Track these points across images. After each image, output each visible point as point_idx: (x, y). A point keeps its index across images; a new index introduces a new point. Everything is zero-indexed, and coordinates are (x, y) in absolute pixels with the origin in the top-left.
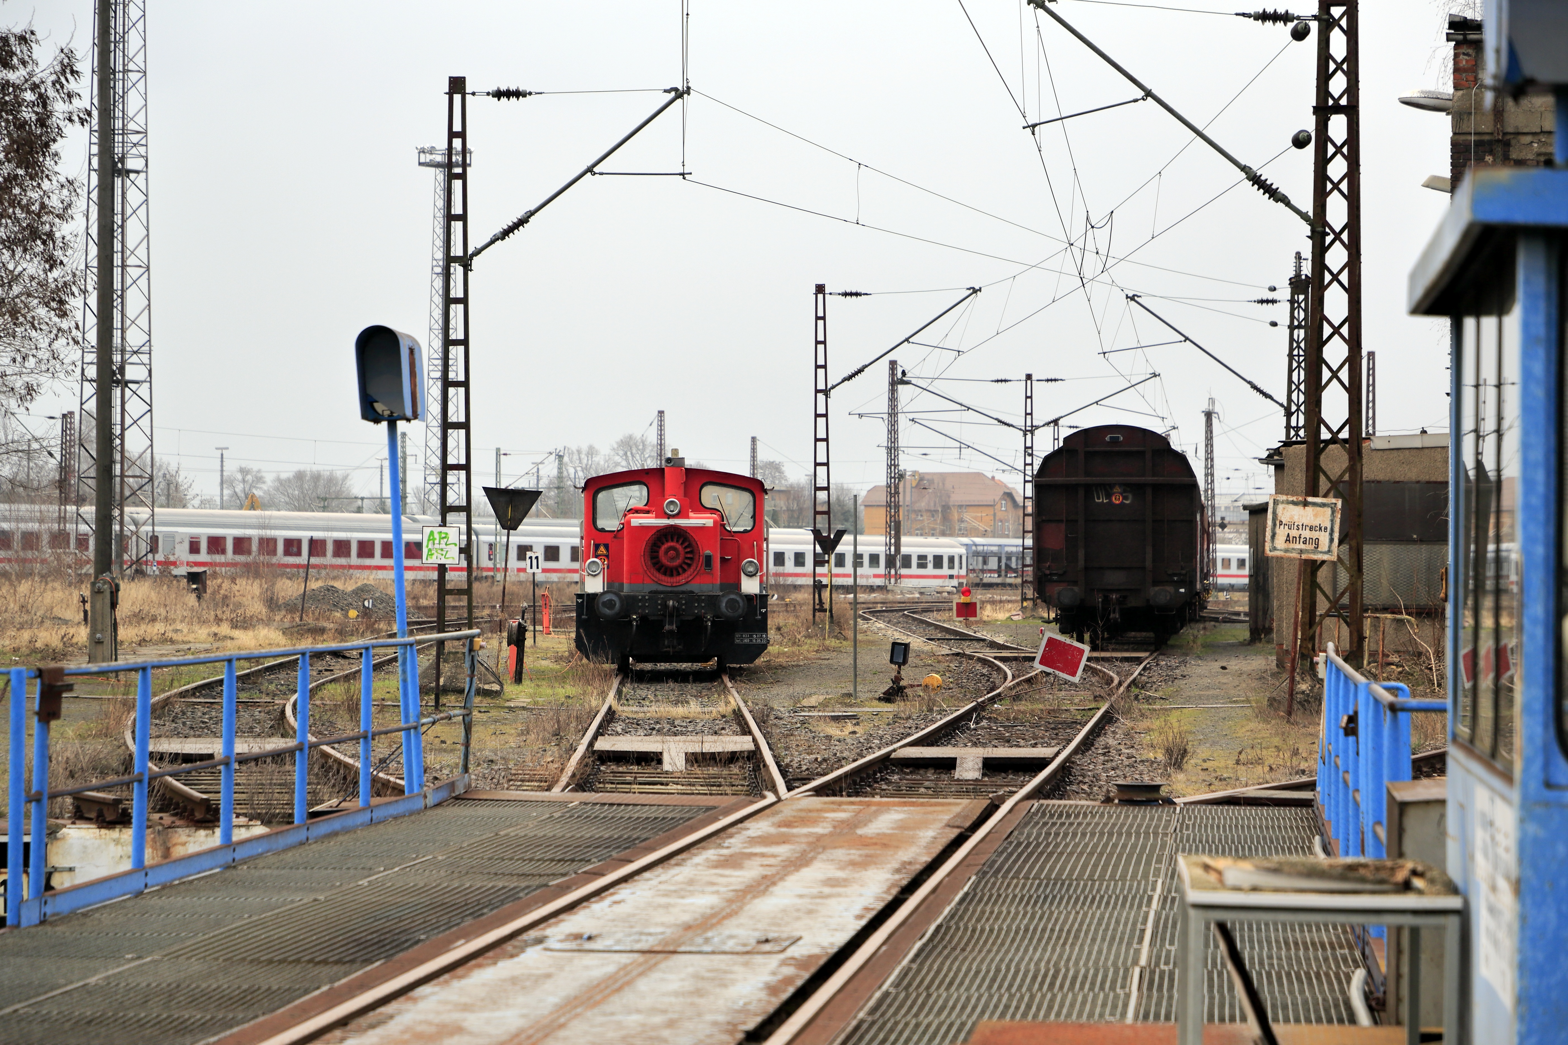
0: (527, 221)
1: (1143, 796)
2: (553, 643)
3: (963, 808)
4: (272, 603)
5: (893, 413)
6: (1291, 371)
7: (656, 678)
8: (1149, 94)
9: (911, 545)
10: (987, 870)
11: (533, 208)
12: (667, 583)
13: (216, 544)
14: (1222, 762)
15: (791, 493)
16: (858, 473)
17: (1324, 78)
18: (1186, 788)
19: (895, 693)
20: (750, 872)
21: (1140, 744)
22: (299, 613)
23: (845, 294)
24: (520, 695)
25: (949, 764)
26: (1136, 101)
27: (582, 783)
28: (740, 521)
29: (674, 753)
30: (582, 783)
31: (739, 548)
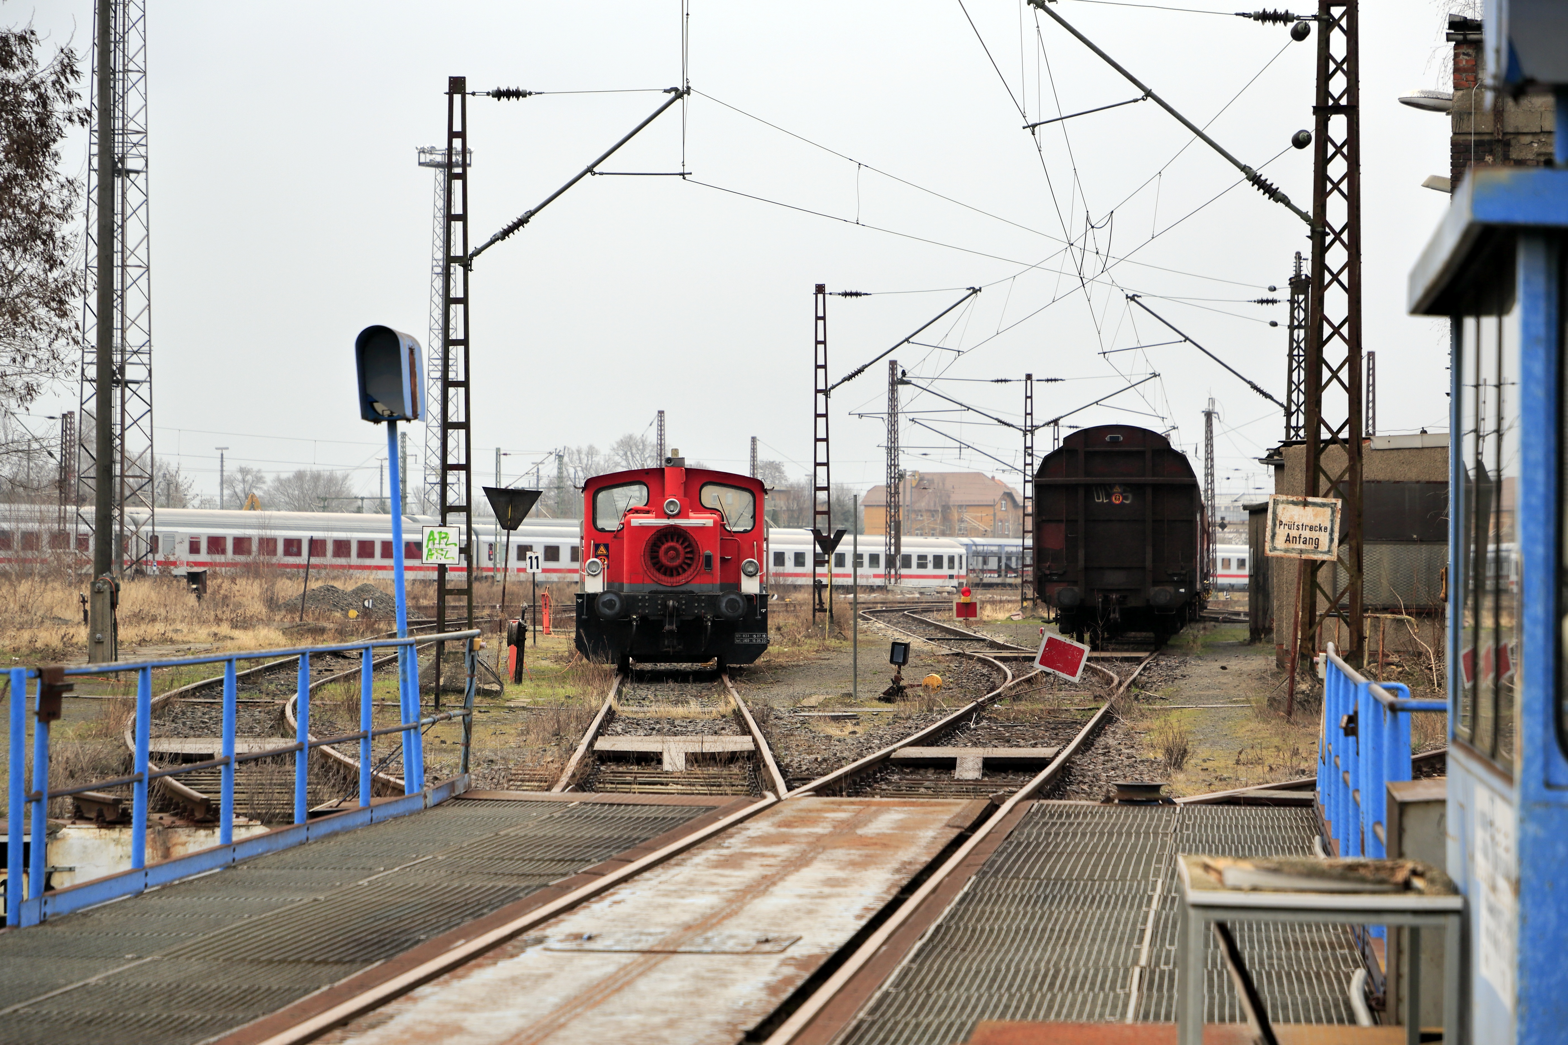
0: (527, 221)
1: (1143, 796)
2: (553, 643)
3: (963, 808)
4: (272, 603)
5: (893, 413)
6: (1291, 371)
7: (656, 678)
8: (1149, 94)
9: (911, 545)
10: (987, 870)
11: (533, 208)
12: (667, 583)
13: (216, 544)
14: (1222, 762)
15: (791, 493)
16: (858, 473)
18: (1186, 788)
19: (895, 693)
20: (750, 872)
21: (1140, 744)
22: (299, 613)
23: (845, 294)
24: (520, 695)
25: (949, 764)
26: (1136, 101)
27: (582, 783)
28: (740, 521)
29: (674, 753)
30: (582, 783)
31: (739, 548)
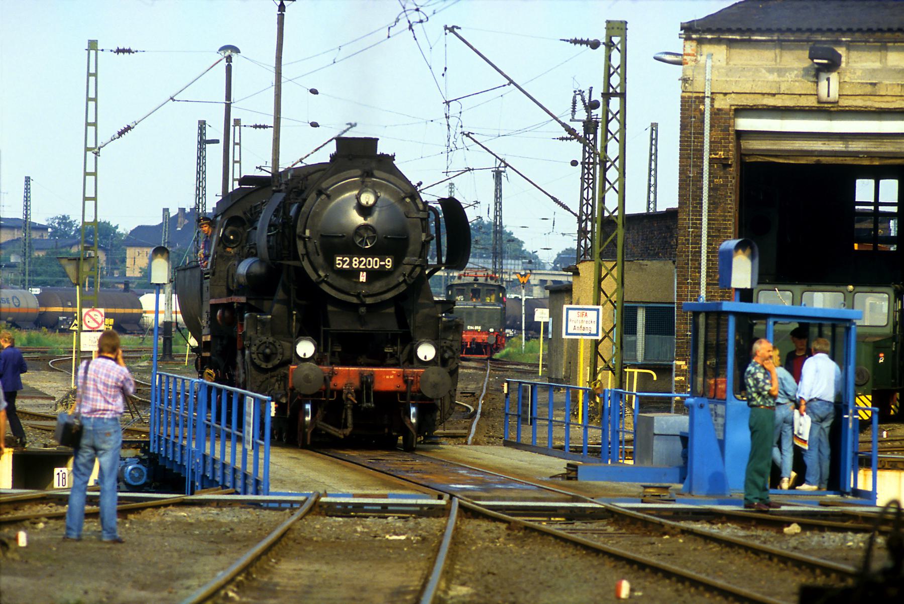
6: (582, 190)
8: (511, 82)
17: (608, 76)
23: (256, 127)
